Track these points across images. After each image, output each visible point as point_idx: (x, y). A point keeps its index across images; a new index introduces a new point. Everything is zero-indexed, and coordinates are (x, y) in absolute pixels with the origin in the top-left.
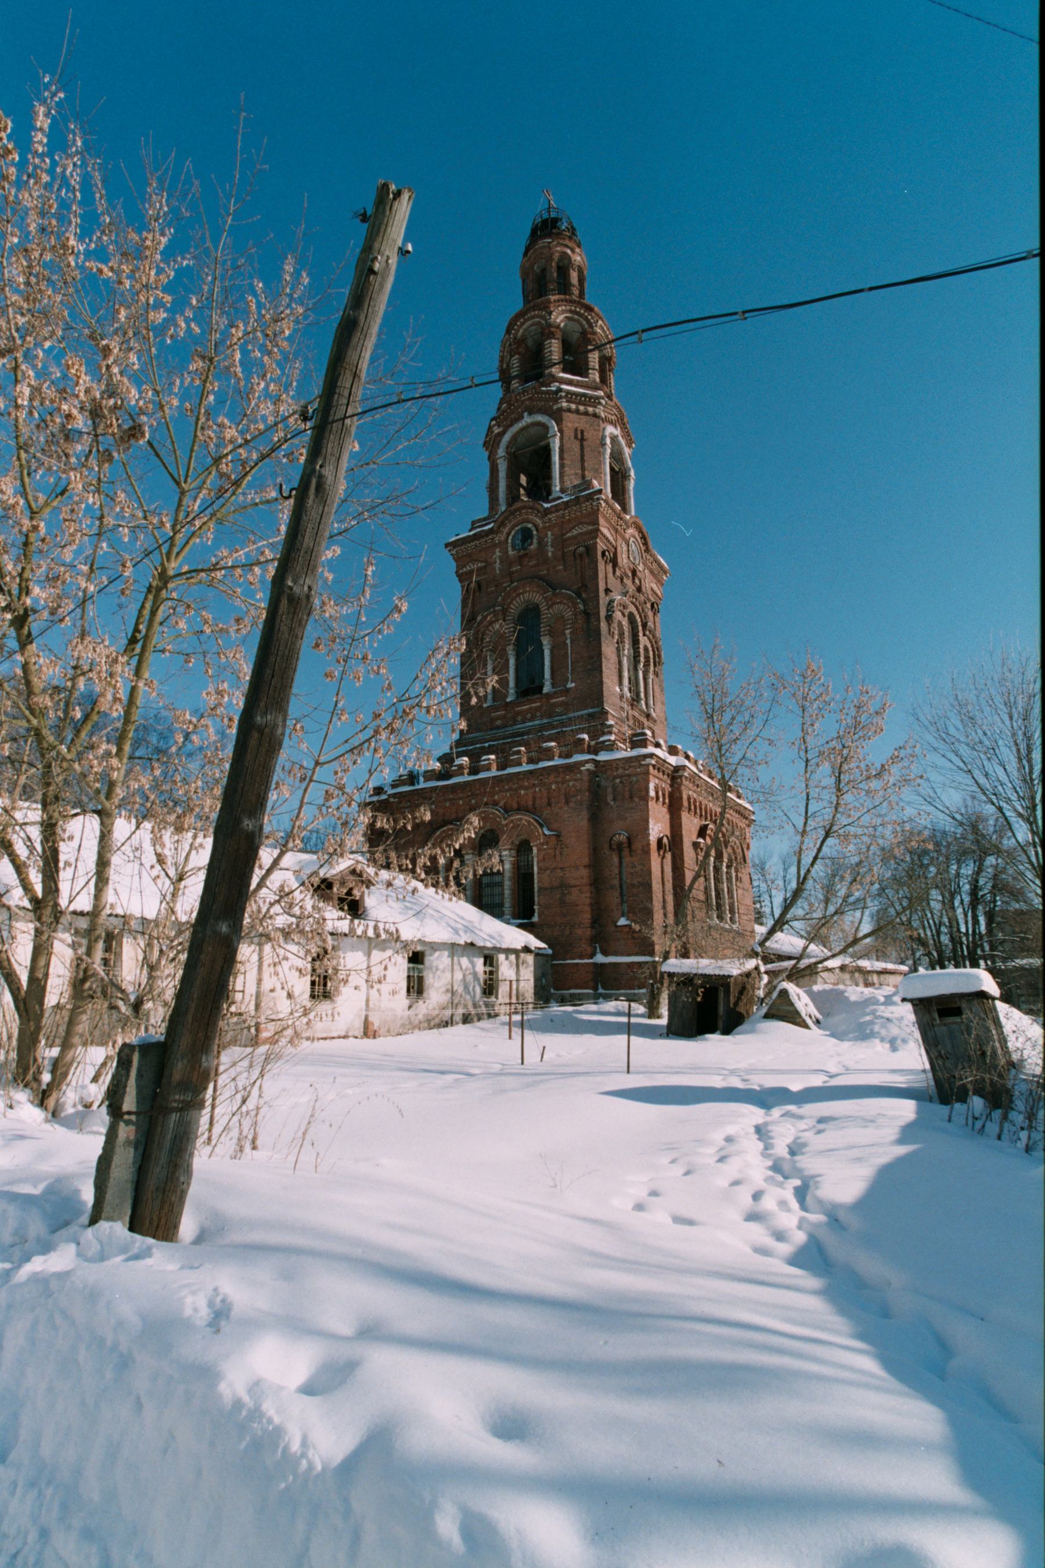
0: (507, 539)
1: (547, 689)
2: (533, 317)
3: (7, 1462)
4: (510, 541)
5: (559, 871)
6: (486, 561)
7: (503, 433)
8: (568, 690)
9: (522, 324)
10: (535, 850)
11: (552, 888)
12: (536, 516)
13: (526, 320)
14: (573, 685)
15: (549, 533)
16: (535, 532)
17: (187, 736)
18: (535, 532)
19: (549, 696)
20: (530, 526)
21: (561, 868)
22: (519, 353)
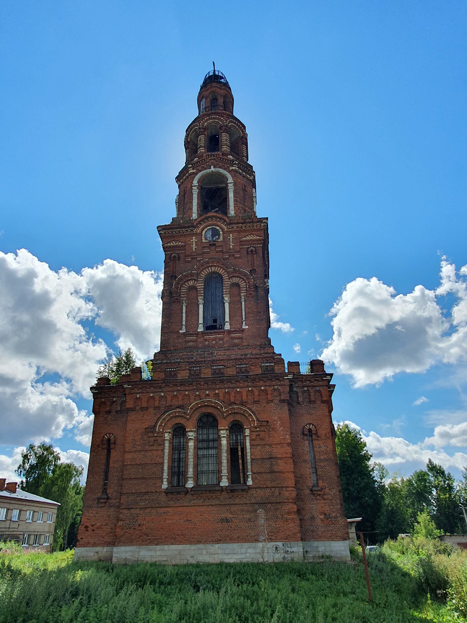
0: (202, 232)
1: (227, 327)
2: (214, 118)
3: (53, 296)
4: (203, 233)
5: (268, 447)
6: (185, 242)
7: (196, 174)
8: (243, 330)
9: (207, 120)
10: (247, 432)
11: (263, 459)
12: (223, 223)
13: (210, 119)
14: (247, 327)
15: (231, 235)
16: (221, 233)
17: (95, 521)
18: (221, 233)
19: (229, 332)
20: (218, 228)
21: (269, 445)
22: (205, 135)
